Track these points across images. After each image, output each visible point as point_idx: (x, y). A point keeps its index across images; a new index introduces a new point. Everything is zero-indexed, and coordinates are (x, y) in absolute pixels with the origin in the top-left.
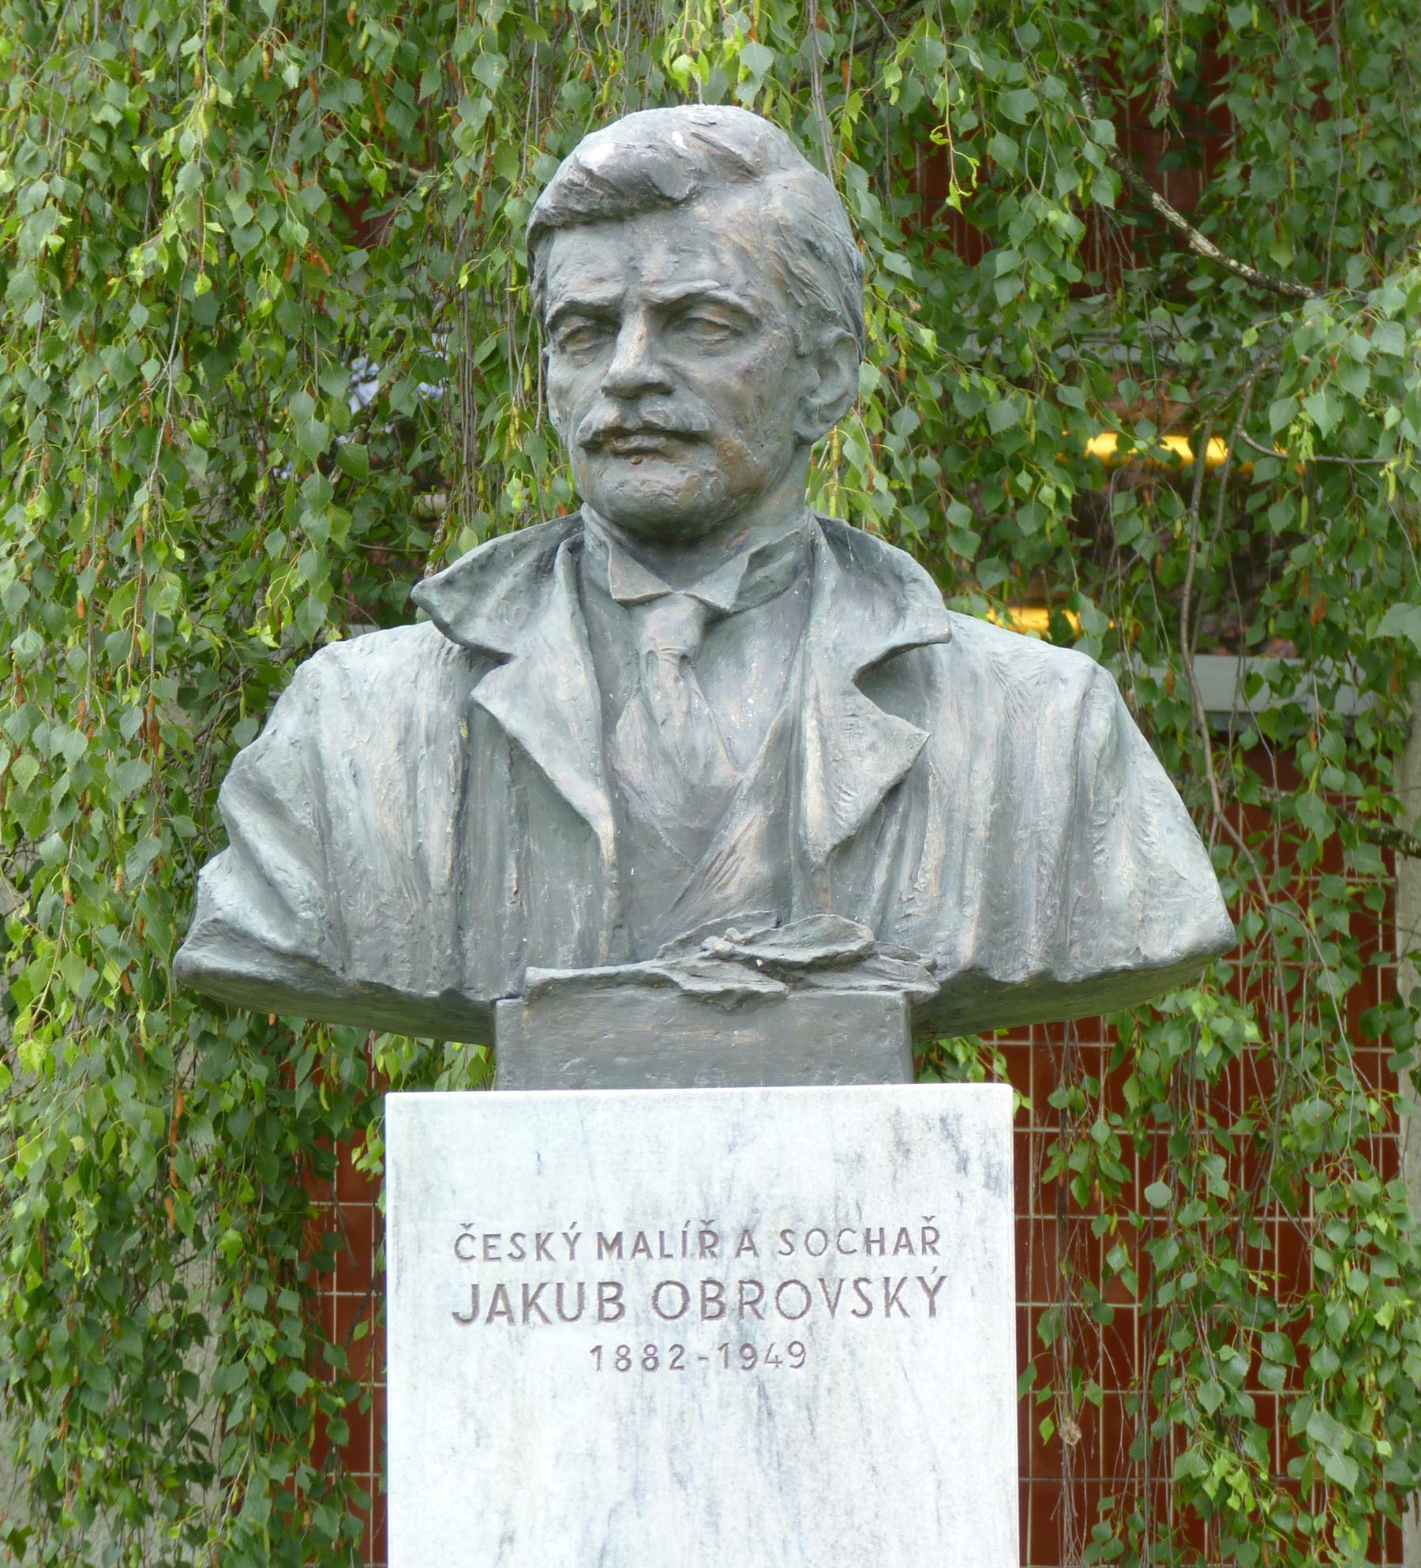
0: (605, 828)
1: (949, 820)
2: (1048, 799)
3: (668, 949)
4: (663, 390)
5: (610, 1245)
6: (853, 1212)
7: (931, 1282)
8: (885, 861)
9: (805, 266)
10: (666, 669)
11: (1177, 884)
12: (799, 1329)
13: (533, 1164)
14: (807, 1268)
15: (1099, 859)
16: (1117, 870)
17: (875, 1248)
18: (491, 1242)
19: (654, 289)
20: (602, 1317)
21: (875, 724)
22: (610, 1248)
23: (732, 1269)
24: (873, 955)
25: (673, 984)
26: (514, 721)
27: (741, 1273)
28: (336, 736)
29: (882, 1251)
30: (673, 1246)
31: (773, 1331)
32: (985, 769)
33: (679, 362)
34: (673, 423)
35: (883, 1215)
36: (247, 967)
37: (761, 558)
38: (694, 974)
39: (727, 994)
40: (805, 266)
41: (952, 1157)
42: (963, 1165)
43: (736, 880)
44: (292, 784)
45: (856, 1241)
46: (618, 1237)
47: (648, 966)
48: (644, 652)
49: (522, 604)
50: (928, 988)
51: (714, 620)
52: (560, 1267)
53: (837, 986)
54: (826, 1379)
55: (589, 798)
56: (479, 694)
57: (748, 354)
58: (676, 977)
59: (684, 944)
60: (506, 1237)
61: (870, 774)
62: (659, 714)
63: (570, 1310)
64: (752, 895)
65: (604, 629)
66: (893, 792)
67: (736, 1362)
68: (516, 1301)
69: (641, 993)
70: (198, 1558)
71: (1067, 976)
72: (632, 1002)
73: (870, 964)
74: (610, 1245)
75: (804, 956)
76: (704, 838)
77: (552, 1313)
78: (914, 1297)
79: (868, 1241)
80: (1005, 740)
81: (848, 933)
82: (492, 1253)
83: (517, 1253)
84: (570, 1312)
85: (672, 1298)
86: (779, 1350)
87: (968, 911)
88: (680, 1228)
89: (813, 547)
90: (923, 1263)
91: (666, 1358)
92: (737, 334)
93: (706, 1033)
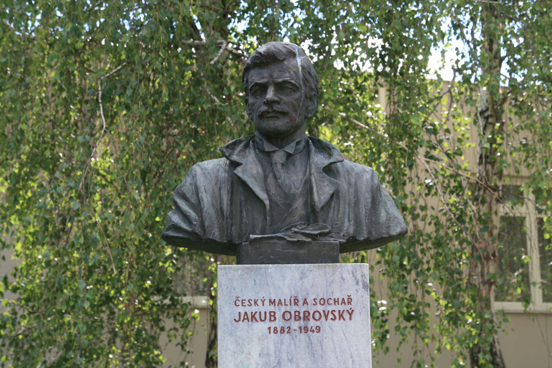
0: (267, 202)
1: (345, 202)
2: (366, 198)
4: (278, 103)
5: (272, 302)
7: (350, 311)
8: (332, 211)
9: (308, 76)
10: (279, 166)
12: (318, 323)
14: (320, 308)
16: (382, 215)
20: (270, 320)
23: (302, 309)
25: (285, 239)
26: (245, 178)
28: (201, 182)
30: (288, 303)
31: (312, 323)
32: (352, 190)
34: (280, 110)
35: (338, 295)
36: (180, 235)
37: (298, 143)
38: (290, 237)
39: (298, 241)
40: (308, 76)
41: (354, 281)
42: (357, 283)
45: (332, 302)
47: (279, 235)
50: (344, 241)
52: (260, 308)
53: (325, 240)
54: (325, 335)
55: (262, 195)
56: (235, 172)
57: (297, 95)
58: (286, 237)
59: (286, 230)
60: (247, 300)
61: (328, 190)
62: (278, 177)
63: (263, 319)
64: (301, 219)
65: (265, 157)
66: (332, 196)
67: (303, 331)
68: (250, 316)
69: (276, 241)
71: (372, 239)
72: (275, 243)
74: (272, 302)
76: (289, 206)
77: (258, 319)
78: (346, 316)
80: (356, 184)
81: (326, 227)
84: (263, 318)
85: (287, 316)
86: (314, 328)
89: (308, 142)
90: (348, 307)
91: (286, 330)
92: (295, 91)
93: (291, 251)
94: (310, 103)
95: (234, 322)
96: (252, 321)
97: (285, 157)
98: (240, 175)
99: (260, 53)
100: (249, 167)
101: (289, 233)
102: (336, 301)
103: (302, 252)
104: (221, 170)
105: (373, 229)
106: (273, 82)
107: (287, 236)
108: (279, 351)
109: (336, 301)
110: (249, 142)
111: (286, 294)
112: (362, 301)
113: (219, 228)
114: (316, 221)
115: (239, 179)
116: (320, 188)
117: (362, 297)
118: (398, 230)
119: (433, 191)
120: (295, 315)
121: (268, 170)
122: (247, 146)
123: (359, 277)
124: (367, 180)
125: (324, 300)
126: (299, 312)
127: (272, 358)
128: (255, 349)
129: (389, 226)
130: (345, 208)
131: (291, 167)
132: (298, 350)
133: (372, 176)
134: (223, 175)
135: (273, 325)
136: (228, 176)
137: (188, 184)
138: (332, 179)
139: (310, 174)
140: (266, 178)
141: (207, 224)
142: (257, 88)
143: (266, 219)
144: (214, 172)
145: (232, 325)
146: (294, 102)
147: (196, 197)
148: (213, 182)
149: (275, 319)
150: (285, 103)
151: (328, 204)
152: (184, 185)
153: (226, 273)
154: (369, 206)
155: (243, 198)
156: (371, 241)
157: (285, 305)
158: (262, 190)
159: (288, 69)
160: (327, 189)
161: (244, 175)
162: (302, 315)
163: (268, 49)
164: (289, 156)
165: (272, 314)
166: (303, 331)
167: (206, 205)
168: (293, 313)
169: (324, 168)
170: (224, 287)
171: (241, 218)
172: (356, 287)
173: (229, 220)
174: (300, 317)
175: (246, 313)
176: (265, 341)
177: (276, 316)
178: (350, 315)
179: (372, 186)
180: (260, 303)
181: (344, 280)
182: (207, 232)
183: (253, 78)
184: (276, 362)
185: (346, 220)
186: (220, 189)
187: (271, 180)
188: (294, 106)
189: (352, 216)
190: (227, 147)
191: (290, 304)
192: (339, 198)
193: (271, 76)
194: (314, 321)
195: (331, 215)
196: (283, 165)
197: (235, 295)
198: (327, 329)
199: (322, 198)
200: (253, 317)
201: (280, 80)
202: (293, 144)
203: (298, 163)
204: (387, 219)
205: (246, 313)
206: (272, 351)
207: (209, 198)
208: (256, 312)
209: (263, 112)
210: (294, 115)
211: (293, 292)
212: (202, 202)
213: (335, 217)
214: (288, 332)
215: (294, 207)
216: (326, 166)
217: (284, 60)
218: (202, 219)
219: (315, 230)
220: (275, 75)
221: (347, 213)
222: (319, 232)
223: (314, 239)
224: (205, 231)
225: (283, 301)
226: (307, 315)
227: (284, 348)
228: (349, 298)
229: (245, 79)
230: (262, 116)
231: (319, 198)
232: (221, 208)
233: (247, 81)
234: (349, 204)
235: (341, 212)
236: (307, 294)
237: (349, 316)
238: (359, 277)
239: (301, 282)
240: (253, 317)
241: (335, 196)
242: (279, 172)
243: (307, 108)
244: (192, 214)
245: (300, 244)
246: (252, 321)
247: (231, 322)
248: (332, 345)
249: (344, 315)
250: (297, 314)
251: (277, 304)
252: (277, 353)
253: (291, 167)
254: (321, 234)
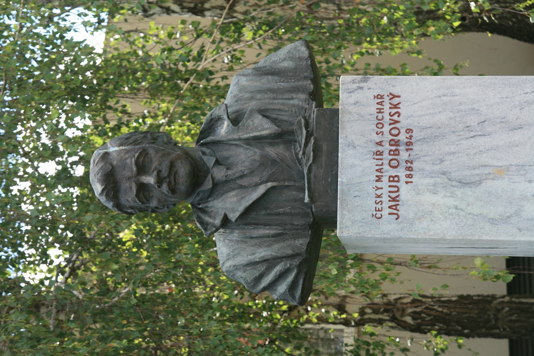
0: (270, 185)
1: (272, 104)
2: (267, 82)
3: (301, 168)
4: (159, 172)
5: (379, 179)
6: (372, 116)
7: (376, 188)
8: (281, 117)
9: (130, 140)
10: (230, 172)
11: (290, 52)
12: (403, 131)
13: (357, 198)
15: (283, 69)
17: (382, 111)
18: (377, 209)
19: (134, 173)
20: (398, 181)
21: (246, 121)
22: (380, 179)
23: (387, 147)
24: (305, 117)
27: (387, 145)
28: (243, 259)
29: (383, 109)
30: (380, 162)
31: (403, 137)
32: (259, 96)
33: (153, 169)
34: (168, 169)
35: (373, 109)
37: (204, 153)
38: (308, 160)
39: (313, 150)
40: (130, 140)
41: (359, 91)
42: (361, 88)
43: (284, 153)
44: (255, 272)
45: (380, 116)
46: (377, 176)
47: (305, 172)
48: (225, 179)
49: (212, 214)
50: (314, 103)
51: (218, 163)
54: (416, 124)
55: (261, 190)
56: (233, 220)
57: (152, 152)
58: (309, 164)
60: (376, 205)
61: (258, 119)
62: (241, 174)
63: (396, 189)
64: (288, 149)
65: (218, 188)
66: (264, 116)
67: (410, 147)
69: (312, 175)
72: (315, 176)
73: (307, 118)
74: (379, 179)
75: (304, 132)
76: (274, 162)
77: (396, 194)
78: (395, 101)
79: (380, 112)
80: (252, 92)
81: (299, 122)
82: (380, 209)
83: (380, 203)
84: (396, 189)
85: (394, 163)
86: (408, 135)
87: (294, 97)
88: (375, 161)
89: (203, 145)
90: (386, 99)
91: (409, 165)
92: (147, 154)
93: (323, 158)
94: (160, 140)
95: (399, 220)
96: (398, 201)
97: (219, 166)
98: (237, 214)
99: (103, 190)
100: (228, 206)
101: (304, 161)
102: (380, 111)
103: (325, 147)
104: (230, 237)
105: (302, 75)
106: (136, 176)
107: (307, 163)
108: (431, 173)
109: (380, 111)
110: (200, 209)
111: (371, 164)
112: (379, 84)
113: (295, 239)
114: (292, 133)
115: (242, 216)
116: (256, 129)
117: (376, 84)
118: (303, 49)
119: (238, 54)
120: (393, 155)
121: (233, 186)
122: (204, 211)
123: (355, 86)
124: (247, 81)
125: (378, 123)
126: (390, 151)
127: (439, 180)
128: (428, 198)
129: (299, 58)
130: (278, 103)
131: (230, 161)
132: (430, 153)
133: (243, 75)
134: (236, 235)
135: (403, 179)
136: (237, 229)
137: (244, 275)
138: (246, 116)
139: (240, 139)
140: (241, 187)
141: (290, 252)
142: (141, 195)
143: (288, 186)
144: (232, 246)
145: (402, 222)
146: (159, 155)
147: (260, 265)
148: (244, 246)
149: (396, 176)
150: (160, 165)
151: (274, 121)
152: (245, 279)
153: (346, 227)
154: (276, 78)
155: (264, 212)
156: (314, 78)
157: (382, 165)
158: (255, 190)
159: (123, 161)
160: (256, 121)
161: (237, 211)
162: (393, 148)
163: (99, 181)
164: (218, 163)
165: (392, 179)
166: (410, 147)
167: (269, 253)
168: (391, 157)
169: (233, 124)
170: (361, 229)
171: (285, 214)
172: (365, 89)
173: (287, 227)
174: (396, 150)
175: (390, 207)
176: (420, 187)
177: (394, 175)
178: (395, 96)
179: (255, 75)
180: (379, 192)
181: (357, 102)
182: (299, 252)
183: (130, 199)
184: (443, 176)
185: (291, 102)
186: (252, 238)
187: (244, 182)
188: (163, 155)
189: (287, 96)
190: (205, 229)
191: (382, 159)
192: (267, 110)
193: (129, 179)
194: (400, 135)
195: (285, 118)
196: (228, 169)
197: (370, 218)
198: (409, 121)
199: (266, 126)
200: (394, 199)
201: (135, 169)
202: (205, 158)
203: (226, 154)
204: (291, 60)
205: (390, 207)
206: (432, 181)
207: (261, 250)
208: (389, 196)
209: (169, 189)
210: (174, 155)
211: (369, 156)
212: (265, 258)
213: (287, 113)
214: (412, 163)
215: (275, 156)
216: (231, 122)
217: (111, 165)
218: (285, 257)
219: (302, 133)
220: (128, 174)
221: (283, 101)
222: (304, 129)
223: (312, 135)
224: (297, 255)
225: (378, 168)
226: (393, 143)
227: (428, 168)
228: (377, 97)
229: (129, 211)
230: (173, 190)
231: (267, 129)
232: (274, 236)
233: (132, 208)
234: (274, 99)
235: (282, 107)
236: (371, 141)
237: (396, 98)
238: (355, 86)
239: (358, 148)
240: (394, 199)
241: (264, 113)
242: (236, 172)
243: (165, 143)
244: (278, 269)
245: (316, 149)
246: (398, 201)
247: (399, 223)
248: (427, 117)
249: (395, 103)
250: (392, 153)
251: (381, 174)
252: (433, 175)
253: (230, 161)
254: (307, 126)
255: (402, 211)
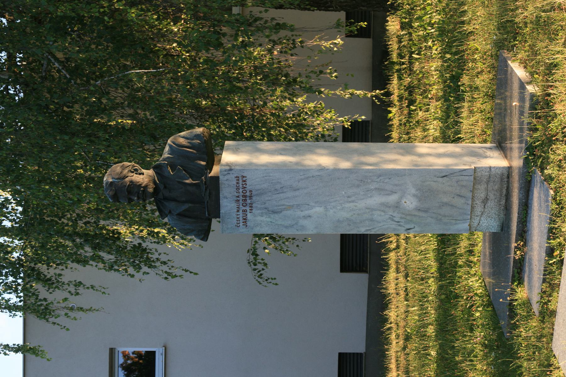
12: (248, 191)
14: (241, 190)
31: (248, 194)
35: (235, 183)
55: (186, 206)
70: (230, 1)
78: (244, 179)
85: (244, 204)
90: (240, 178)
111: (234, 205)
128: (259, 218)
245: (210, 194)
255: (248, 224)
